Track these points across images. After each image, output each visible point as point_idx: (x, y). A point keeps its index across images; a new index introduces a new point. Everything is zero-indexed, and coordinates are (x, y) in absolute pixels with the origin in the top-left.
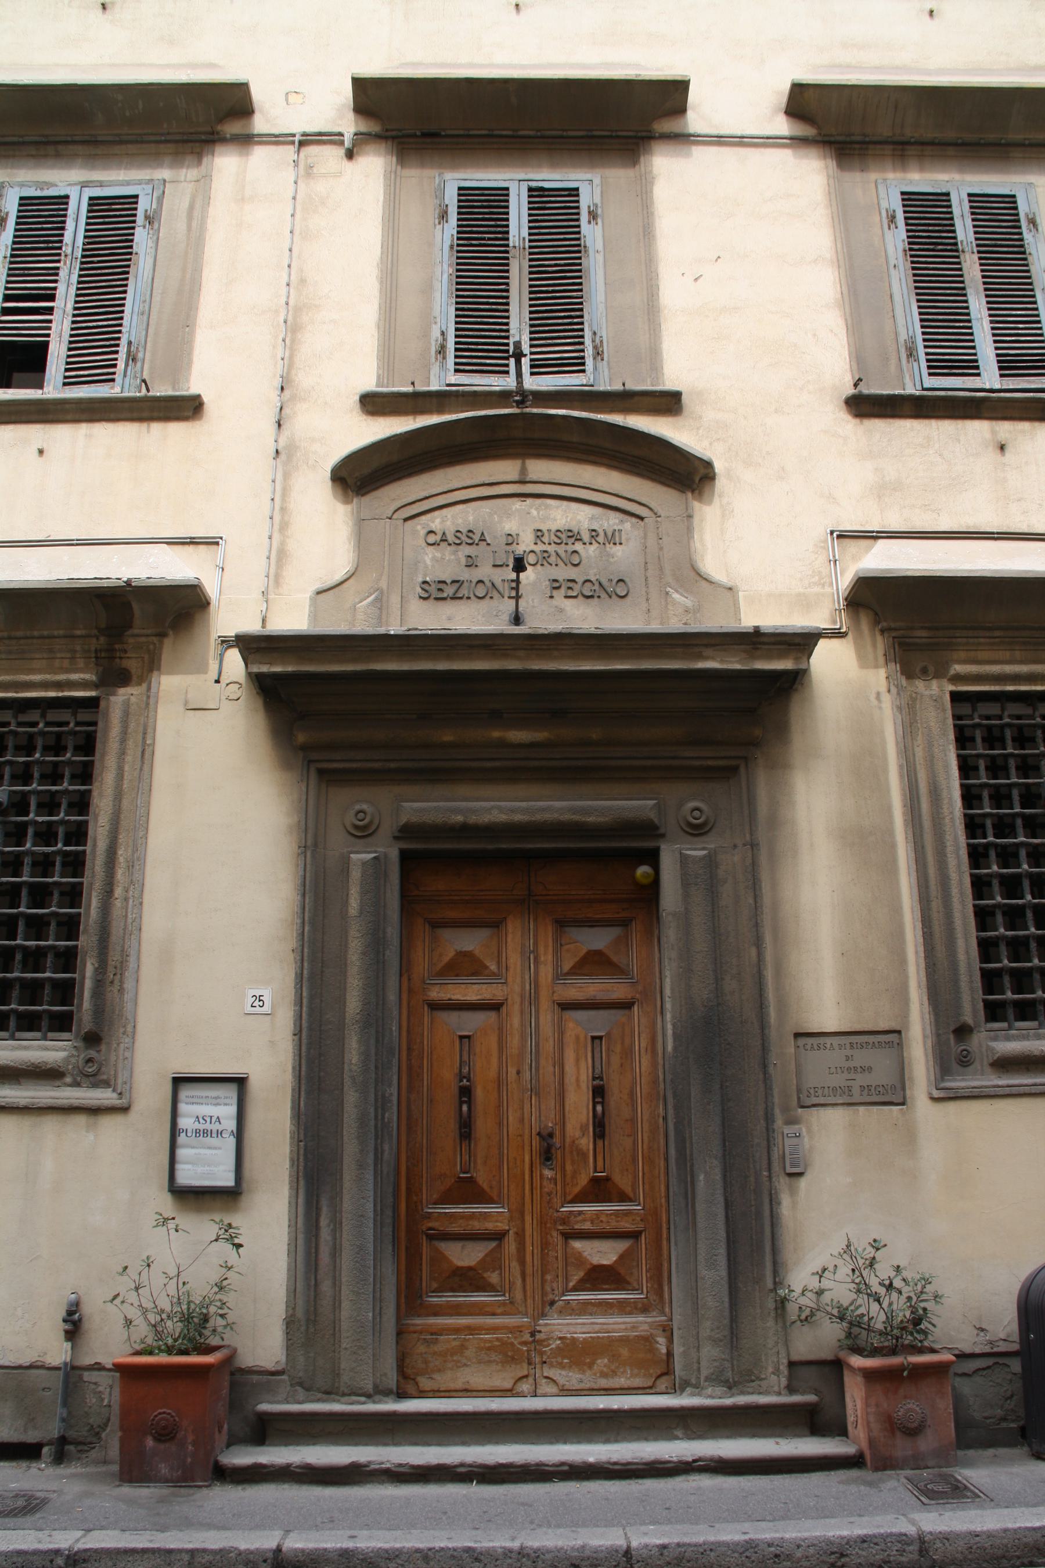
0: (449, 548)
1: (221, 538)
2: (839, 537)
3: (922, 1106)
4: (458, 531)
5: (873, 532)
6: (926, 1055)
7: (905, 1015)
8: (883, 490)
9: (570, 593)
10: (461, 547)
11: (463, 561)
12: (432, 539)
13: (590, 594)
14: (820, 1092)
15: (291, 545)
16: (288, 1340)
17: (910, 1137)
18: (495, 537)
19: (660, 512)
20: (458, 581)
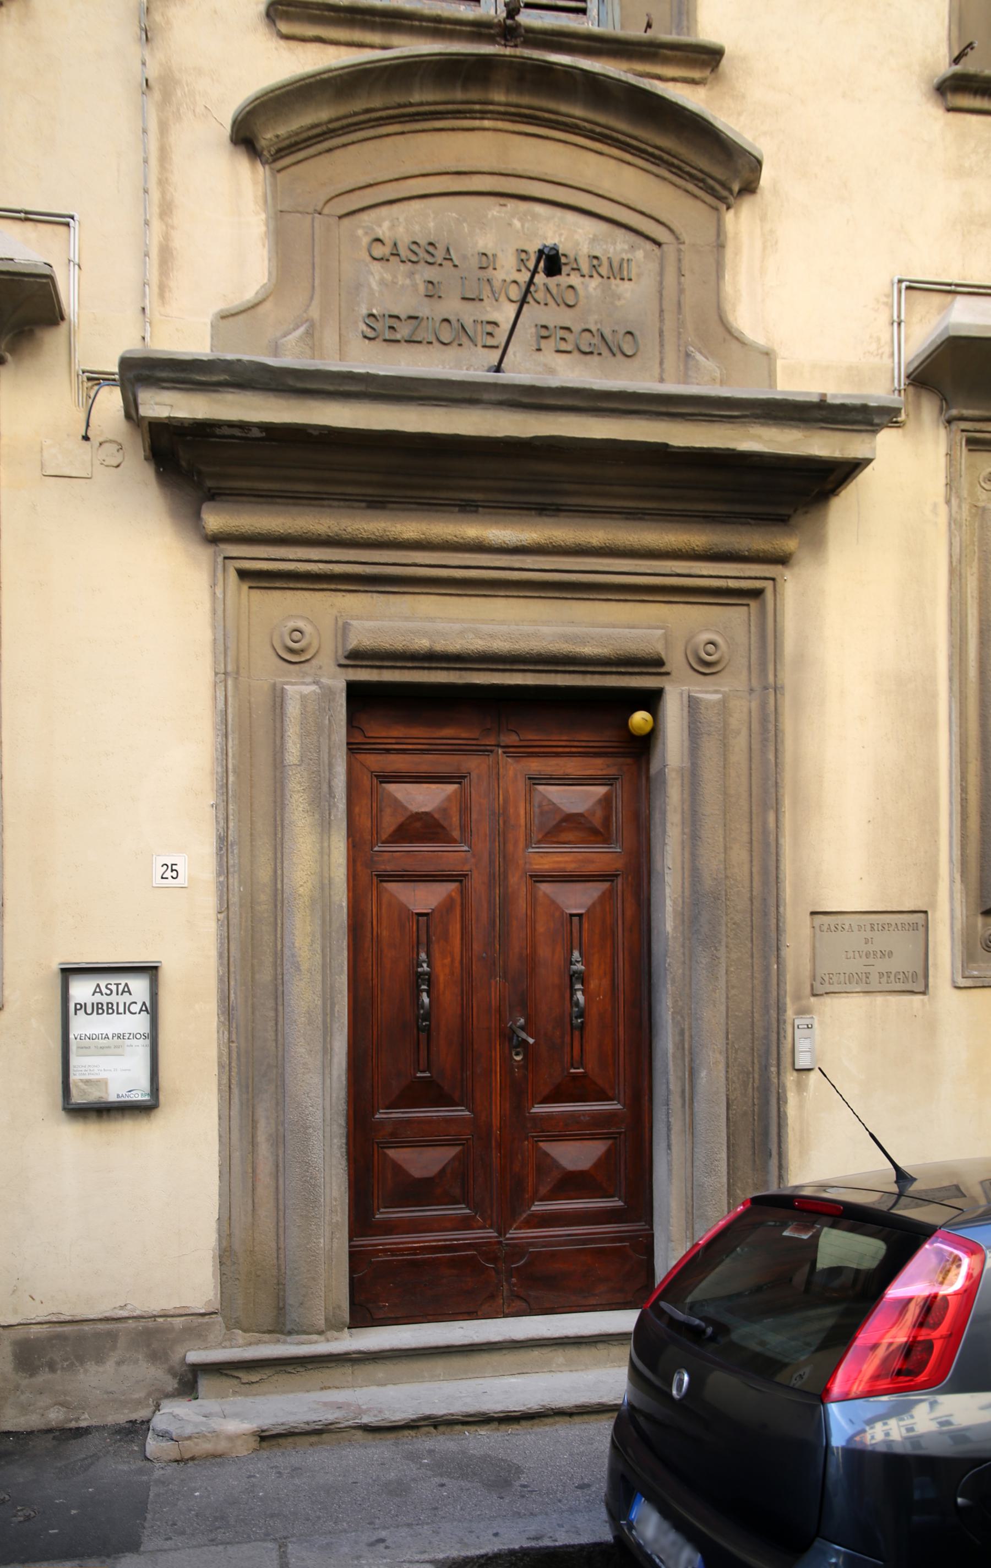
0: (402, 266)
1: (72, 218)
2: (908, 288)
3: (947, 1000)
4: (415, 243)
5: (950, 285)
6: (953, 939)
7: (933, 894)
8: (974, 223)
9: (563, 346)
10: (418, 267)
11: (422, 288)
12: (379, 251)
13: (588, 350)
14: (835, 979)
15: (178, 242)
16: (222, 1274)
17: (931, 1026)
18: (464, 257)
19: (685, 237)
20: (416, 318)
